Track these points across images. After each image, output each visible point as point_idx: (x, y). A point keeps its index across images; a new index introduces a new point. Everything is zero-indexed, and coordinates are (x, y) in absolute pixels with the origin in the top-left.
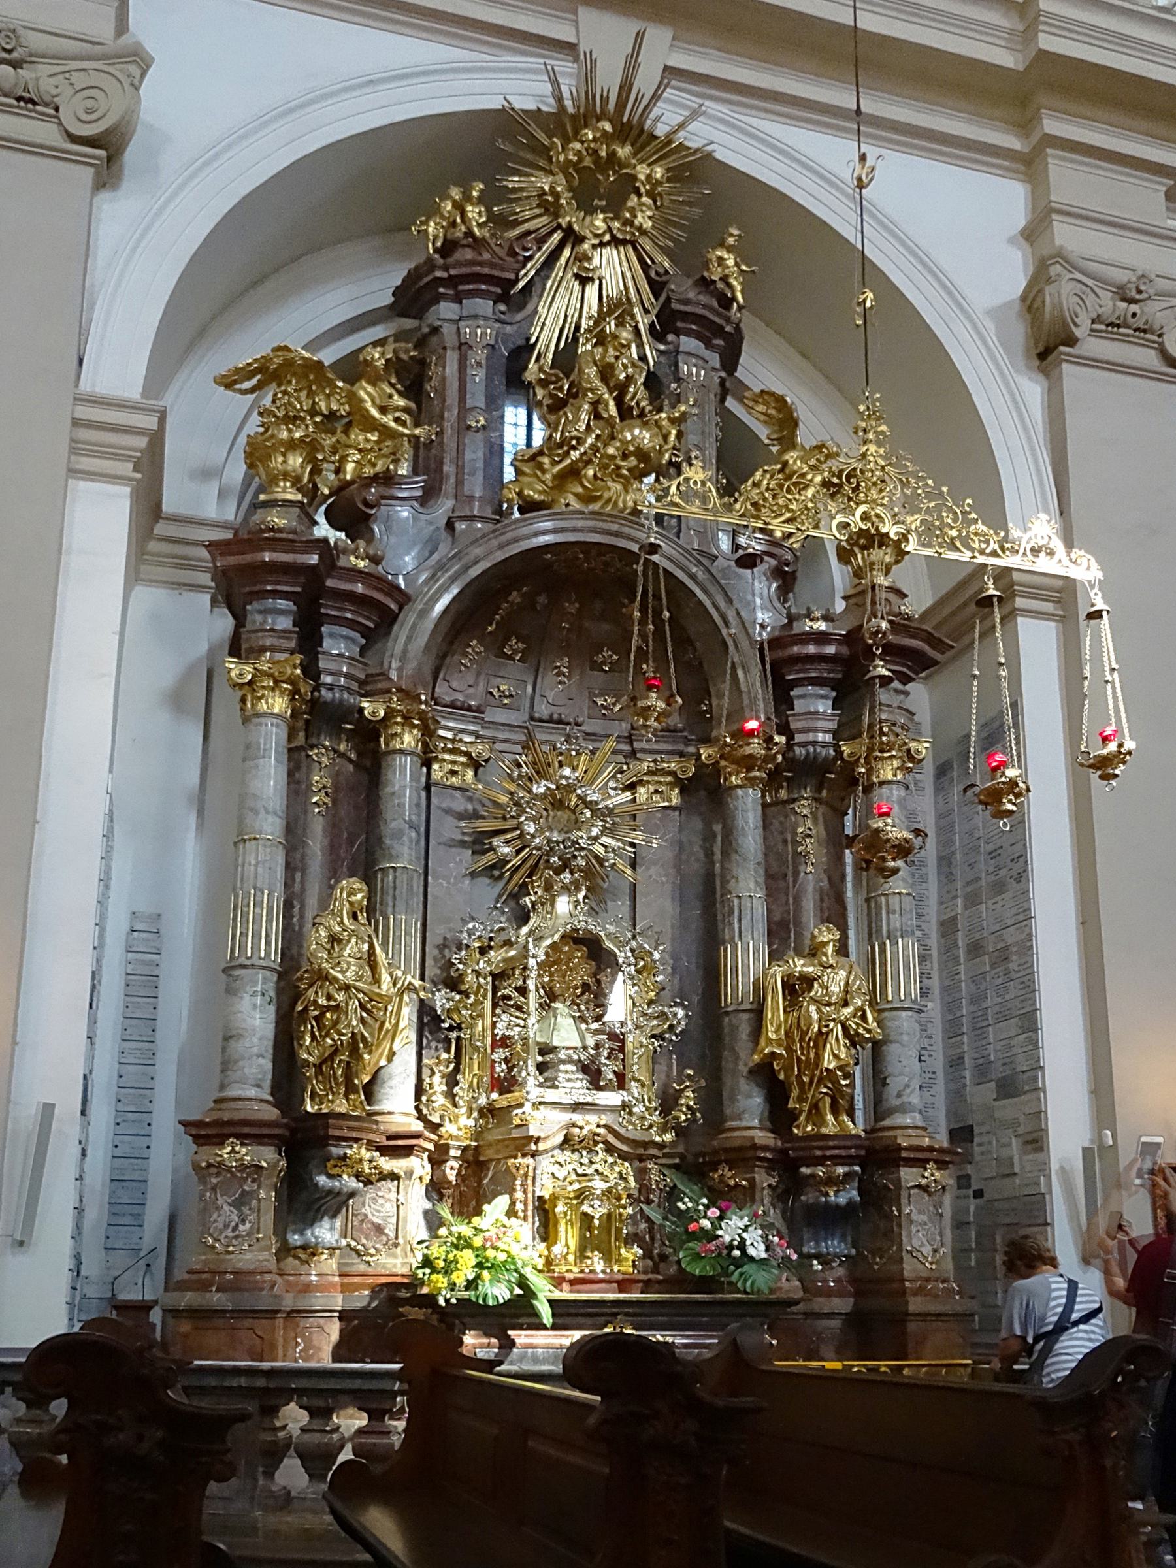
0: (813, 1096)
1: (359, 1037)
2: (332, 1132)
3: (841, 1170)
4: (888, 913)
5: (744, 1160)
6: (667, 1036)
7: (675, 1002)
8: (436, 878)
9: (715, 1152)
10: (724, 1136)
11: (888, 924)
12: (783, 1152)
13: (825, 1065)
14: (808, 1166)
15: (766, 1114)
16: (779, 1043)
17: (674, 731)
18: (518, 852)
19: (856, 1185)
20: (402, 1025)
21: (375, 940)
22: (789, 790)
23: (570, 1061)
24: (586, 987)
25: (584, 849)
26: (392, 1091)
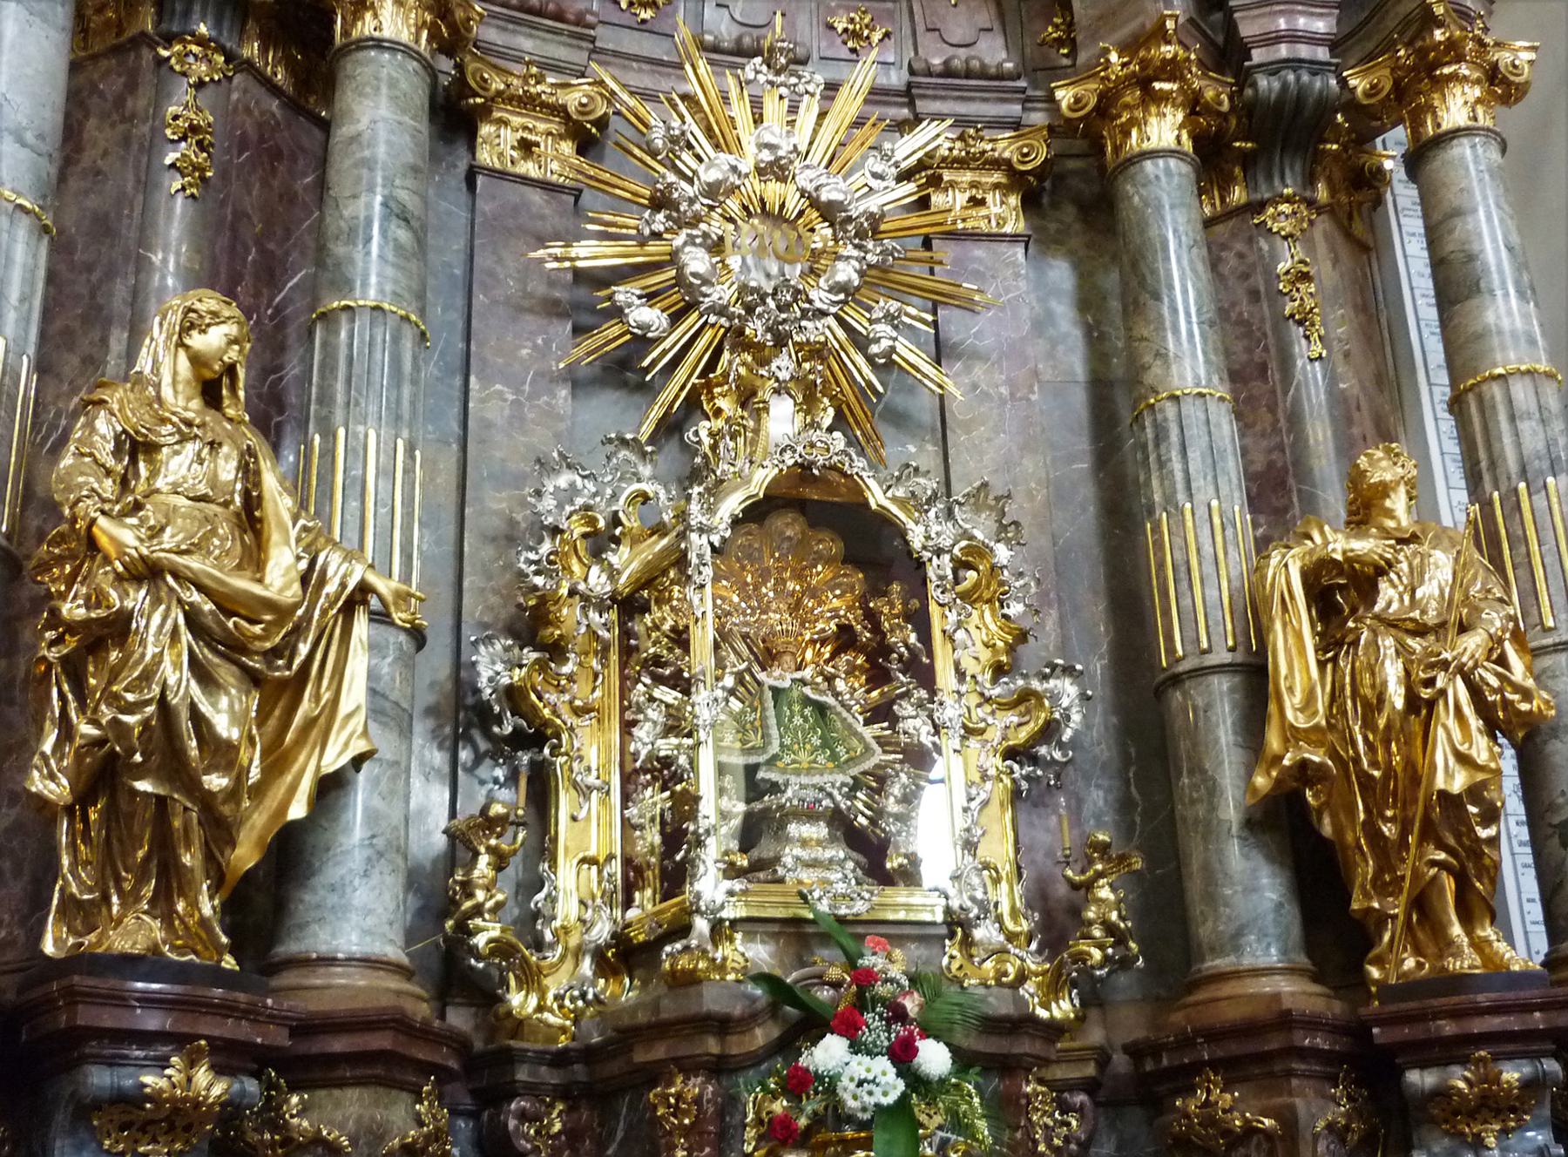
0: (1415, 871)
1: (186, 725)
2: (88, 1016)
3: (1512, 1074)
4: (1512, 418)
5: (1264, 1058)
6: (1043, 750)
7: (1054, 667)
8: (486, 381)
9: (1185, 1042)
10: (1201, 995)
11: (1518, 444)
12: (1357, 1031)
13: (1440, 782)
14: (1423, 1066)
15: (1296, 931)
16: (1313, 736)
17: (1000, 77)
18: (676, 318)
19: (1547, 1112)
20: (344, 708)
21: (266, 466)
22: (1251, 184)
23: (810, 816)
24: (844, 639)
25: (824, 314)
26: (333, 899)
